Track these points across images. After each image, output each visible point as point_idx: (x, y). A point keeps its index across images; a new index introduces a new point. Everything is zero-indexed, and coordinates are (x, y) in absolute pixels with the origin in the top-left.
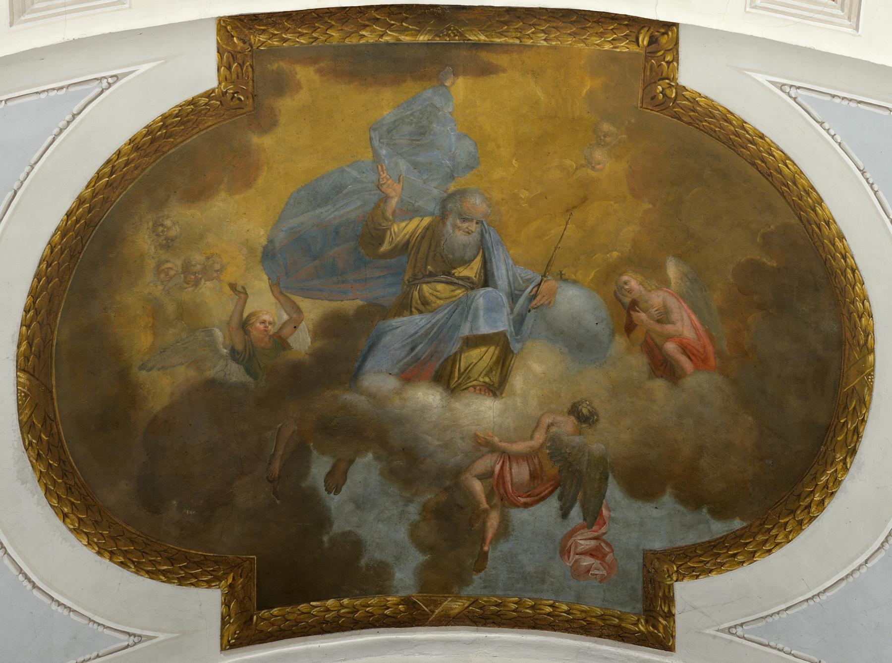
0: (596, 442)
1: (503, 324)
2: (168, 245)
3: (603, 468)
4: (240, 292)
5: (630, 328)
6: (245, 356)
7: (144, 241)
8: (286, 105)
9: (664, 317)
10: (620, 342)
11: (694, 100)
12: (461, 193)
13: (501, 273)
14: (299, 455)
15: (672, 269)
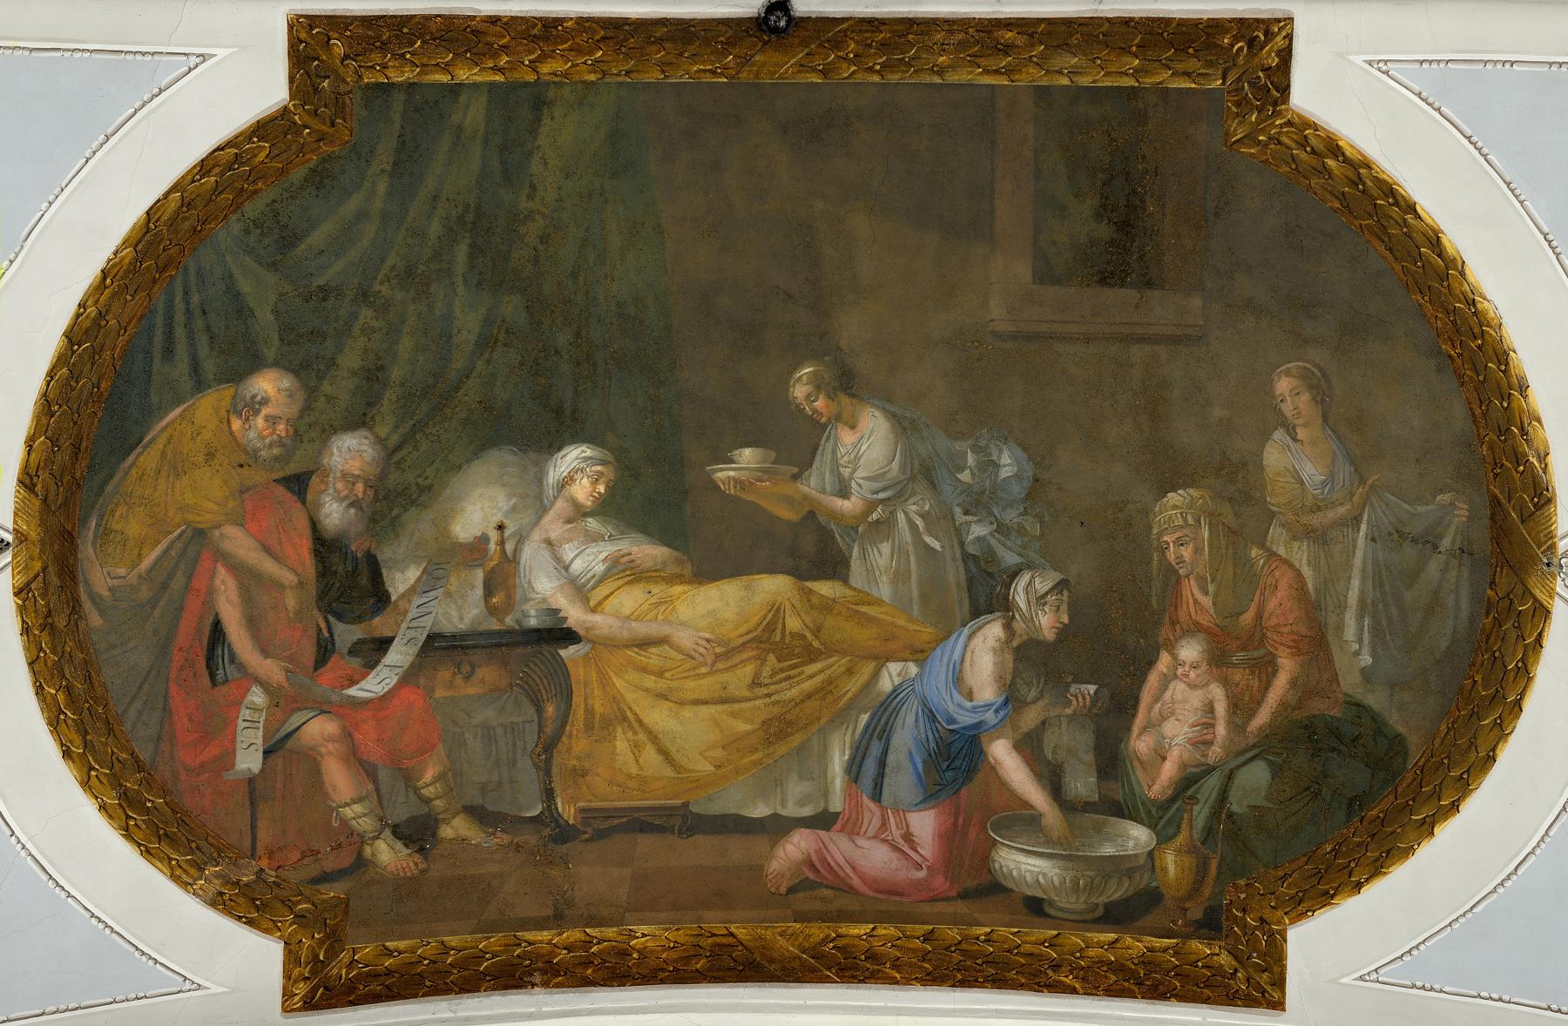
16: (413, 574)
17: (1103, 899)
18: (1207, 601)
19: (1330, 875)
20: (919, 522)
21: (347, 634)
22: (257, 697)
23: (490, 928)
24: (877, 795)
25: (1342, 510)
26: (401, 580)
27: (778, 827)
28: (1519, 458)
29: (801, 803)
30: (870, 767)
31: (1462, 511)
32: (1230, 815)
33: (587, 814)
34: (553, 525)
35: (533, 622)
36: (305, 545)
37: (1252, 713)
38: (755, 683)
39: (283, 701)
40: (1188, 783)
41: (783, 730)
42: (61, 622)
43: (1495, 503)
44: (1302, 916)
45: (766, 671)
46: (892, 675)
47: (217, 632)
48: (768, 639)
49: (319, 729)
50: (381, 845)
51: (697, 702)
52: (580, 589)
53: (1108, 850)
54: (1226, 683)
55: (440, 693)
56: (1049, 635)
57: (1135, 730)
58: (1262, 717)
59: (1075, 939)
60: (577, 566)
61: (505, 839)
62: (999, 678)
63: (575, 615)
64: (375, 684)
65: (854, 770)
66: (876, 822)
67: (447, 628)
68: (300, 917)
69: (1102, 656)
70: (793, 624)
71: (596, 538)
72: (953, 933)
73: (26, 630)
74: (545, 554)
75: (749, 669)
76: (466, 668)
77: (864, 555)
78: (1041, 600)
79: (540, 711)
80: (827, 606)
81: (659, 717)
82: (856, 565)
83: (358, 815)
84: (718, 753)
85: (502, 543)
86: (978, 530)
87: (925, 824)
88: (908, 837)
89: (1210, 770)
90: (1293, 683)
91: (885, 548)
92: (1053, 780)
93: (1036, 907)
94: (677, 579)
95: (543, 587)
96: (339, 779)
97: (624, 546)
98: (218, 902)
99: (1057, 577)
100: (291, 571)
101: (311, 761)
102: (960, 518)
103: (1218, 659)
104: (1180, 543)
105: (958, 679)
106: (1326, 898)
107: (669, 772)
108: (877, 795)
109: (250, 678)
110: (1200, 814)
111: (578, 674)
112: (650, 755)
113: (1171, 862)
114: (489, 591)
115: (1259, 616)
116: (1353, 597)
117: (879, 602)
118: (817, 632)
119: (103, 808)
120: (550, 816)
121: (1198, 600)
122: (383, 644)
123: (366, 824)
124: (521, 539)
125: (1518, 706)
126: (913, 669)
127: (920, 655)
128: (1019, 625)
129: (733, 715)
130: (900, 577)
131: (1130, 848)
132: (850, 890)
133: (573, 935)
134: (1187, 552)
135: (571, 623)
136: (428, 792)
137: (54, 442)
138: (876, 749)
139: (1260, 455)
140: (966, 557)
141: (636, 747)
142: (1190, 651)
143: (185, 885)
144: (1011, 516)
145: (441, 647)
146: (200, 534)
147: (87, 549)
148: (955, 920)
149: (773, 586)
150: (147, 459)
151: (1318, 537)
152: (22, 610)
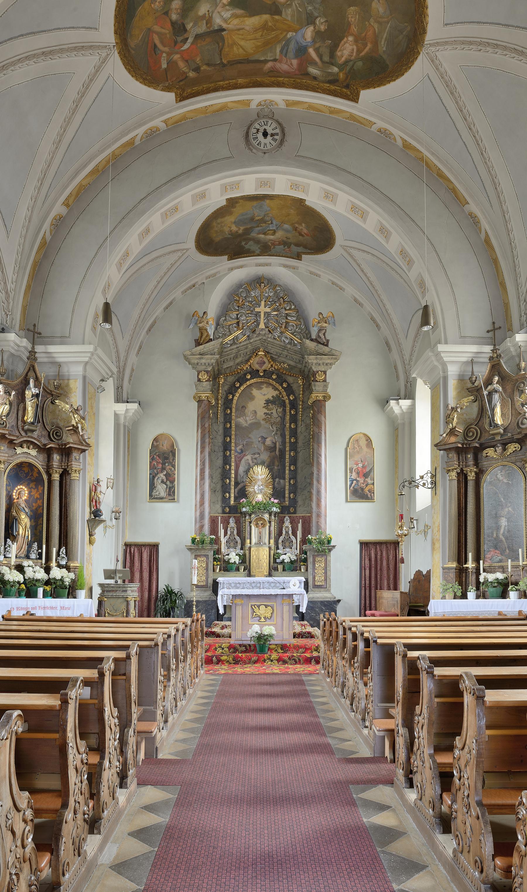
0: (289, 241)
1: (274, 228)
2: (218, 224)
3: (291, 243)
4: (230, 227)
5: (296, 230)
6: (232, 234)
7: (214, 224)
8: (237, 205)
9: (302, 230)
10: (294, 232)
11: (308, 206)
12: (268, 214)
13: (274, 222)
14: (240, 242)
15: (303, 225)
16: (191, 24)
17: (328, 79)
18: (356, 30)
19: (369, 85)
20: (298, 5)
21: (180, 39)
22: (164, 55)
23: (212, 83)
24: (286, 56)
25: (386, 19)
26: (189, 26)
27: (266, 62)
28: (422, 22)
29: (270, 57)
30: (285, 51)
31: (409, 28)
32: (354, 69)
33: (229, 62)
34: (219, 9)
35: (216, 28)
36: (169, 24)
37: (361, 53)
38: (262, 36)
39: (169, 54)
40: (346, 62)
41: (268, 45)
42: (127, 55)
43: (416, 29)
44: (364, 89)
45: (264, 33)
46: (290, 35)
47: (155, 46)
48: (264, 27)
49: (176, 57)
50: (190, 73)
51: (250, 40)
52: (225, 21)
53: (330, 71)
54: (357, 46)
55: (199, 45)
56: (323, 30)
57: (338, 50)
58: (363, 54)
59: (322, 85)
60: (225, 16)
61: (213, 68)
62: (312, 37)
63: (224, 26)
64: (186, 46)
65: (281, 52)
66: (285, 61)
67: (199, 33)
68: (177, 88)
69: (333, 36)
70: (270, 24)
71: (228, 10)
72: (299, 81)
73: (121, 59)
74: (218, 15)
75: (261, 33)
76: (203, 40)
77: (285, 11)
78: (322, 24)
79: (218, 44)
80: (277, 21)
81: (242, 43)
82: (283, 13)
83: (185, 69)
84: (254, 49)
85: (209, 14)
86: (310, 8)
87: (295, 62)
88: (291, 64)
89: (351, 61)
90: (370, 49)
91: (290, 10)
92: (320, 57)
93: (315, 78)
94: (246, 16)
95: (218, 21)
96: (182, 65)
97: (234, 11)
98: (162, 90)
99: (326, 19)
100: (167, 31)
101: (176, 63)
102: (306, 5)
103: (356, 41)
104: (352, 17)
105: (303, 37)
106: (369, 88)
107: (244, 53)
108: (286, 56)
109: (163, 52)
110: (348, 68)
111: (226, 37)
112: (241, 50)
113: (341, 75)
114: (207, 24)
115: (366, 35)
116: (384, 37)
117: (288, 21)
118: (275, 26)
119: (140, 82)
120: (222, 63)
121: (354, 29)
122: (187, 39)
123: (187, 70)
124: (213, 12)
125: (410, 67)
126: (294, 34)
127: (296, 31)
128: (317, 27)
129: (257, 42)
130: (293, 16)
131: (334, 71)
132: (279, 72)
133: (227, 82)
134: (353, 20)
135: (224, 27)
136: (198, 63)
137: (119, 23)
138: (286, 48)
139: (371, 4)
140: (307, 13)
141: (238, 48)
142: (351, 38)
143: (156, 89)
144: (317, 6)
145: (198, 37)
146: (149, 29)
147: (129, 40)
148: (299, 79)
149: (266, 17)
150: (136, 19)
151: (380, 23)
152: (120, 56)
